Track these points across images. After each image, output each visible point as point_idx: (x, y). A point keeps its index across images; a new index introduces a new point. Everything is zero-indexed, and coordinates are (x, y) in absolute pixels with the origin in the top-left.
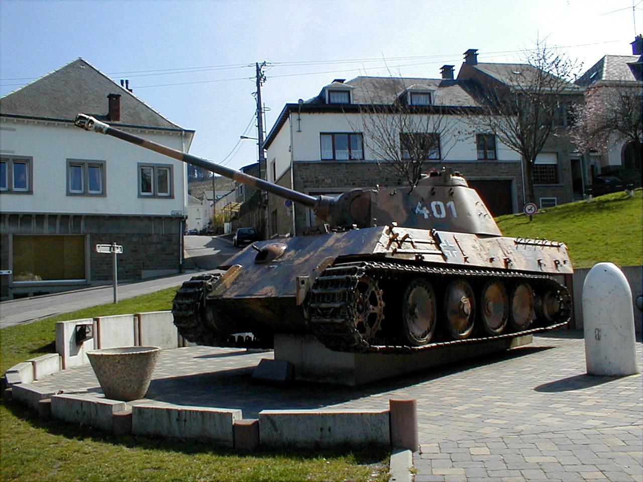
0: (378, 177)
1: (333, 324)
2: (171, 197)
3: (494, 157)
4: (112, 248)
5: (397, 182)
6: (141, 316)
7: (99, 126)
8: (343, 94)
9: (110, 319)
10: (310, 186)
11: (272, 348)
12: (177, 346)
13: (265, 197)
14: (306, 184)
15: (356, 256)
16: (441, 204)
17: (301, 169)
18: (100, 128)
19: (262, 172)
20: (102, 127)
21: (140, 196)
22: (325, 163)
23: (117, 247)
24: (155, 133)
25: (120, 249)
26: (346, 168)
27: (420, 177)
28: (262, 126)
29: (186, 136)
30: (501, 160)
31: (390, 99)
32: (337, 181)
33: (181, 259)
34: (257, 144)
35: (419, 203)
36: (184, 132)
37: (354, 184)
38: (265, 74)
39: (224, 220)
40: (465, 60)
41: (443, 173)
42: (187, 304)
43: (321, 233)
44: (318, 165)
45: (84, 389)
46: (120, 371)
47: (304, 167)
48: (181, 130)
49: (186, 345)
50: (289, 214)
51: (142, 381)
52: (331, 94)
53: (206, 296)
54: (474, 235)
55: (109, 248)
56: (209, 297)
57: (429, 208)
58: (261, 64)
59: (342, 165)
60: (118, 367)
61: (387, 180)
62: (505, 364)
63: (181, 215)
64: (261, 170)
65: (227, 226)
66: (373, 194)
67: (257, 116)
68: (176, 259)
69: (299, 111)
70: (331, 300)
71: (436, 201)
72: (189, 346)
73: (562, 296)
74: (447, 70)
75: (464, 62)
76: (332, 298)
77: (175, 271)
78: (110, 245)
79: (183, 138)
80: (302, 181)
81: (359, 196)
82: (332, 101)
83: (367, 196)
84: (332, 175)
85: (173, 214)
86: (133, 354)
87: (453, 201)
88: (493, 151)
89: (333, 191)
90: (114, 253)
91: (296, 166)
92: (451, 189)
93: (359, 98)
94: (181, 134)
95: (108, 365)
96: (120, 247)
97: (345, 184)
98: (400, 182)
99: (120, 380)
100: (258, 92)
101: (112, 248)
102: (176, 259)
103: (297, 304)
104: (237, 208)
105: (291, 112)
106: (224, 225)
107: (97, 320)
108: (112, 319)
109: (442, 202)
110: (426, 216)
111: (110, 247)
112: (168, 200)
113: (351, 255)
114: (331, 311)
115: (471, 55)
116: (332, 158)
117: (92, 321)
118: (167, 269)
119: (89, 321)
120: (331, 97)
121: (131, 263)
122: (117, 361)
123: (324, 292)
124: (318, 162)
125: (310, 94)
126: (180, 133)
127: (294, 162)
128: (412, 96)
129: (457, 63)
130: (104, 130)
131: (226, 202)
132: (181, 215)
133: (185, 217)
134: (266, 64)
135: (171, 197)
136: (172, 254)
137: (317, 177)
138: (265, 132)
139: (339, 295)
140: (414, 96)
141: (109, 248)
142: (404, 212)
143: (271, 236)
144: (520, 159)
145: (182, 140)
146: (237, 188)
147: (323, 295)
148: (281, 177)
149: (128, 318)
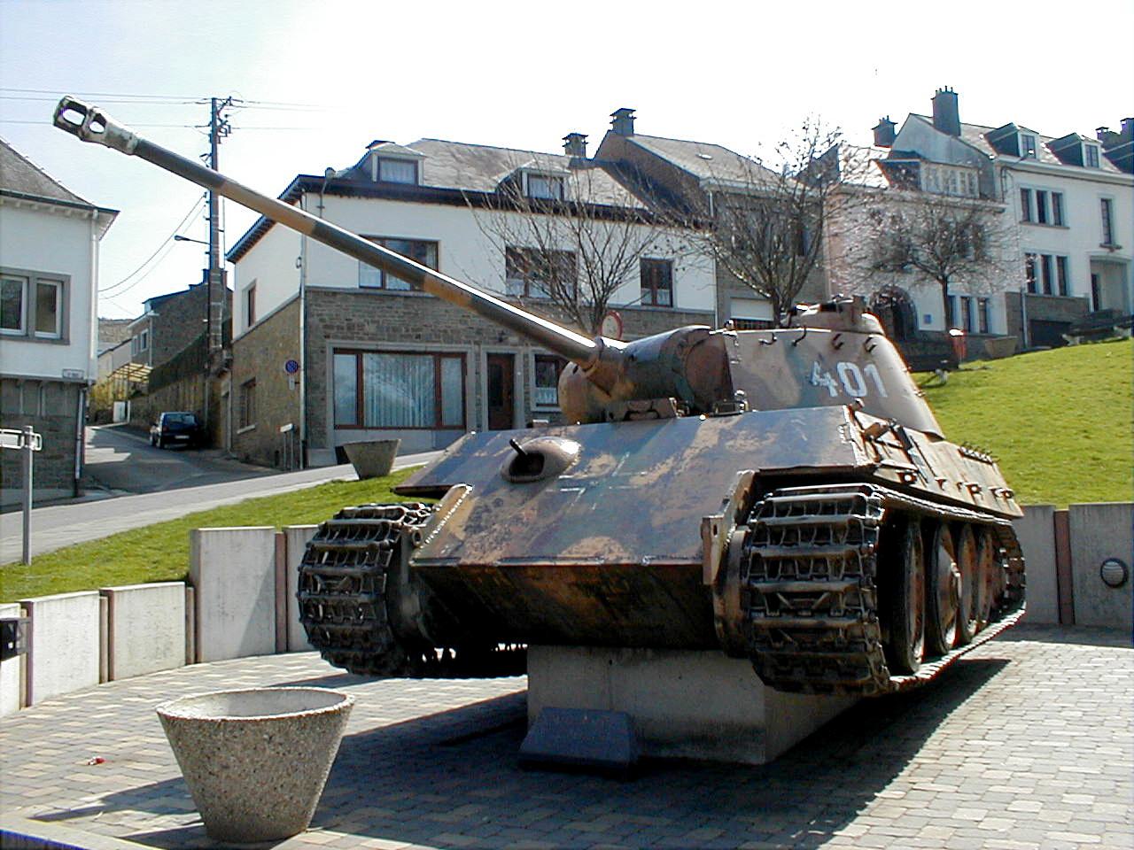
0: (464, 327)
1: (821, 630)
2: (63, 340)
3: (668, 303)
4: (23, 438)
5: (498, 336)
6: (116, 597)
7: (118, 133)
8: (405, 166)
9: (53, 603)
10: (336, 337)
11: (525, 673)
12: (184, 663)
13: (222, 355)
14: (328, 331)
15: (809, 471)
17: (319, 302)
18: (121, 137)
19: (214, 306)
20: (127, 137)
22: (368, 294)
23: (33, 436)
24: (36, 208)
25: (36, 439)
26: (406, 306)
27: (794, 312)
28: (217, 219)
29: (99, 221)
30: (682, 309)
31: (485, 184)
32: (388, 330)
33: (78, 468)
34: (207, 253)
35: (816, 364)
36: (96, 211)
37: (418, 337)
39: (111, 396)
40: (611, 127)
41: (848, 308)
42: (352, 578)
43: (659, 417)
44: (353, 298)
45: (94, 801)
46: (269, 763)
47: (327, 299)
48: (91, 208)
49: (202, 660)
50: (292, 386)
51: (315, 784)
52: (382, 163)
53: (408, 560)
54: (923, 435)
55: (16, 437)
56: (416, 561)
57: (836, 376)
59: (398, 299)
60: (268, 751)
61: (479, 332)
63: (82, 378)
64: (213, 304)
65: (118, 409)
66: (728, 341)
67: (208, 198)
69: (322, 192)
70: (811, 573)
71: (846, 361)
72: (208, 662)
74: (575, 142)
75: (609, 131)
76: (817, 567)
77: (63, 492)
78: (20, 432)
79: (93, 223)
80: (321, 325)
81: (701, 342)
82: (384, 177)
83: (717, 344)
84: (379, 316)
85: (66, 375)
86: (308, 715)
87: (874, 363)
88: (668, 291)
89: (379, 348)
90: (29, 449)
91: (311, 296)
93: (436, 175)
94: (91, 215)
95: (239, 747)
96: (38, 437)
97: (402, 336)
98: (504, 337)
99: (266, 787)
101: (23, 438)
103: (705, 583)
104: (140, 374)
105: (306, 191)
106: (112, 406)
107: (27, 607)
108: (58, 603)
111: (20, 435)
112: (54, 346)
115: (623, 118)
116: (379, 285)
117: (19, 609)
118: (47, 487)
119: (12, 610)
120: (383, 170)
122: (266, 736)
123: (789, 554)
124: (354, 292)
125: (344, 159)
126: (86, 213)
127: (306, 287)
128: (531, 180)
130: (130, 145)
131: (110, 365)
132: (82, 378)
133: (90, 383)
134: (232, 102)
135: (63, 340)
136: (60, 457)
137: (350, 320)
139: (837, 562)
140: (533, 181)
141: (16, 437)
142: (793, 382)
143: (236, 429)
144: (713, 309)
145: (90, 227)
146: (136, 337)
147: (788, 561)
148: (272, 317)
149: (90, 599)
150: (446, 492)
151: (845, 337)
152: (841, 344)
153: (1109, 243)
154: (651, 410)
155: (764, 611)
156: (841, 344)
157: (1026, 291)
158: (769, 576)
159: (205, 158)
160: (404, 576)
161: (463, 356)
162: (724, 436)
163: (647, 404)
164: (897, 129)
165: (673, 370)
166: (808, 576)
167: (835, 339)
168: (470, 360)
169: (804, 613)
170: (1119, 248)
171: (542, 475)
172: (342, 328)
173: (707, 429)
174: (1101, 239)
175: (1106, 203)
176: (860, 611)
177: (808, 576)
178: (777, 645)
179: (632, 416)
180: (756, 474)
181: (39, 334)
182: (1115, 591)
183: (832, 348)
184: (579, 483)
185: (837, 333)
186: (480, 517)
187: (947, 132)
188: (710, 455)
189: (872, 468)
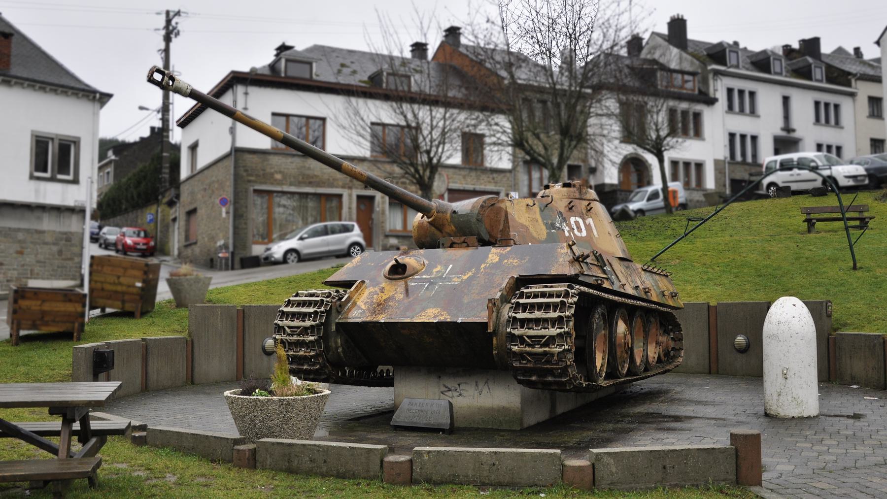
15: (545, 277)
16: (580, 221)
21: (32, 177)
31: (360, 78)
38: (179, 27)
57: (569, 225)
58: (173, 12)
62: (414, 420)
68: (76, 267)
73: (674, 332)
82: (290, 73)
92: (589, 204)
93: (323, 73)
94: (94, 97)
100: (167, 51)
102: (76, 267)
109: (580, 217)
110: (567, 234)
113: (539, 275)
114: (544, 340)
115: (453, 33)
121: (14, 269)
129: (434, 43)
136: (71, 259)
138: (172, 104)
150: (354, 284)
151: (576, 202)
152: (573, 206)
153: (788, 129)
154: (464, 242)
155: (518, 345)
156: (573, 206)
157: (728, 159)
158: (520, 328)
159: (160, 52)
160: (333, 328)
161: (340, 196)
162: (502, 257)
163: (463, 238)
164: (644, 42)
165: (477, 220)
166: (539, 328)
167: (570, 203)
168: (345, 199)
169: (537, 346)
170: (794, 131)
171: (405, 275)
172: (260, 176)
173: (493, 254)
174: (780, 123)
175: (786, 100)
176: (564, 345)
177: (539, 328)
178: (524, 362)
179: (455, 245)
180: (517, 278)
181: (60, 177)
182: (739, 355)
183: (567, 209)
184: (425, 280)
185: (570, 200)
186: (373, 297)
187: (677, 46)
188: (495, 266)
189: (577, 275)
